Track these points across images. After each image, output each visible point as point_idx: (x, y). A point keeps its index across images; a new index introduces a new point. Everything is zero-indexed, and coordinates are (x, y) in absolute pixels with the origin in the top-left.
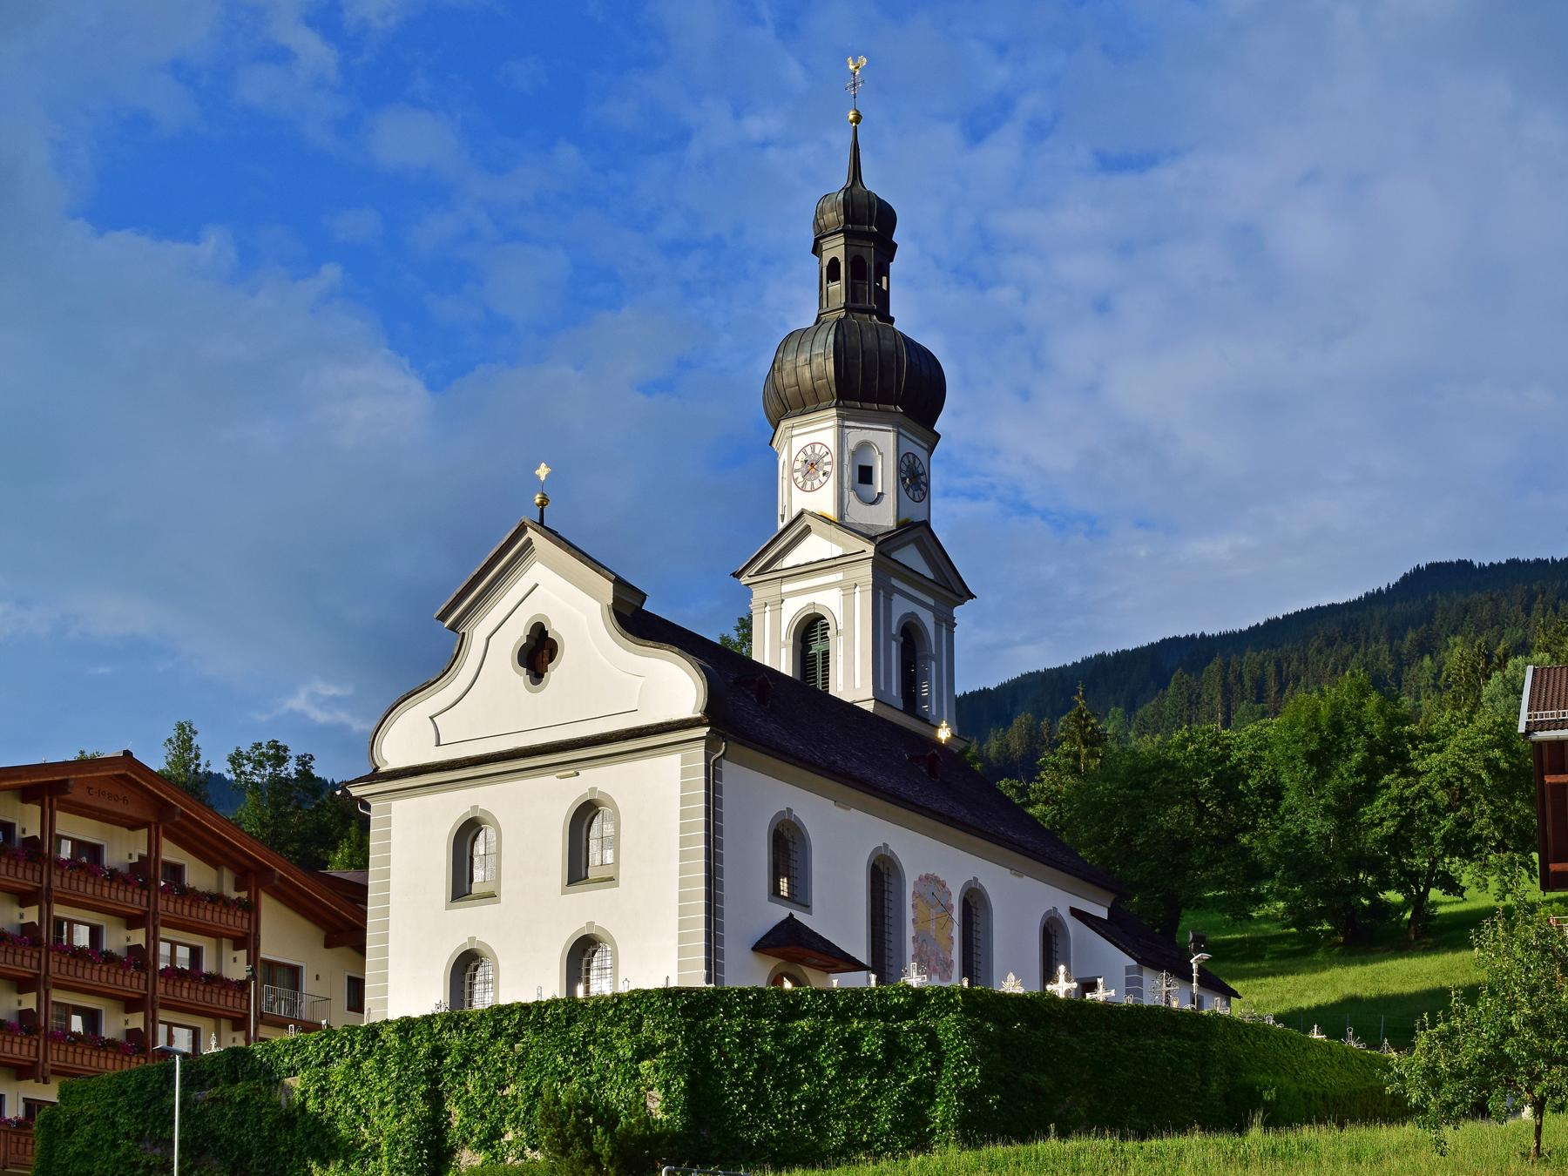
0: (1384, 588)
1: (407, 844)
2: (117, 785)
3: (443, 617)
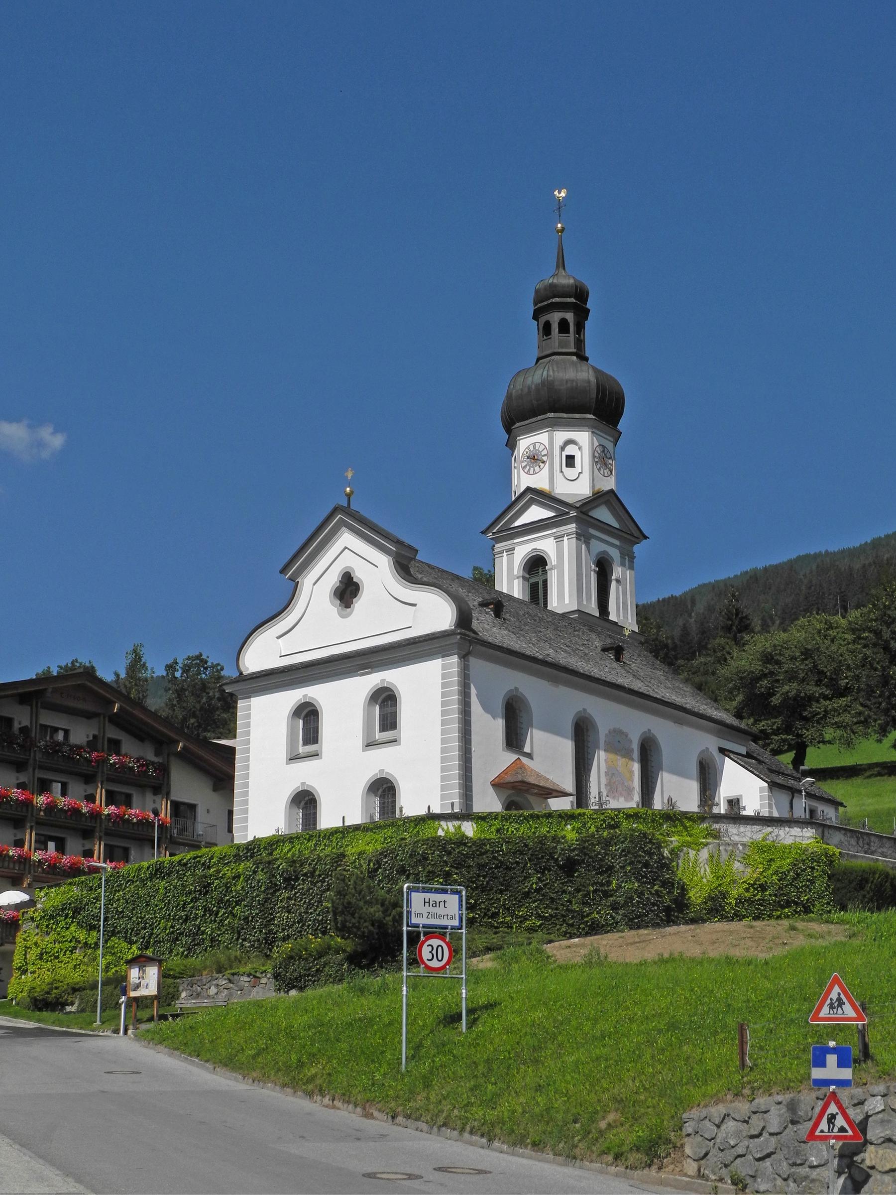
1: (264, 721)
2: (77, 688)
3: (283, 571)
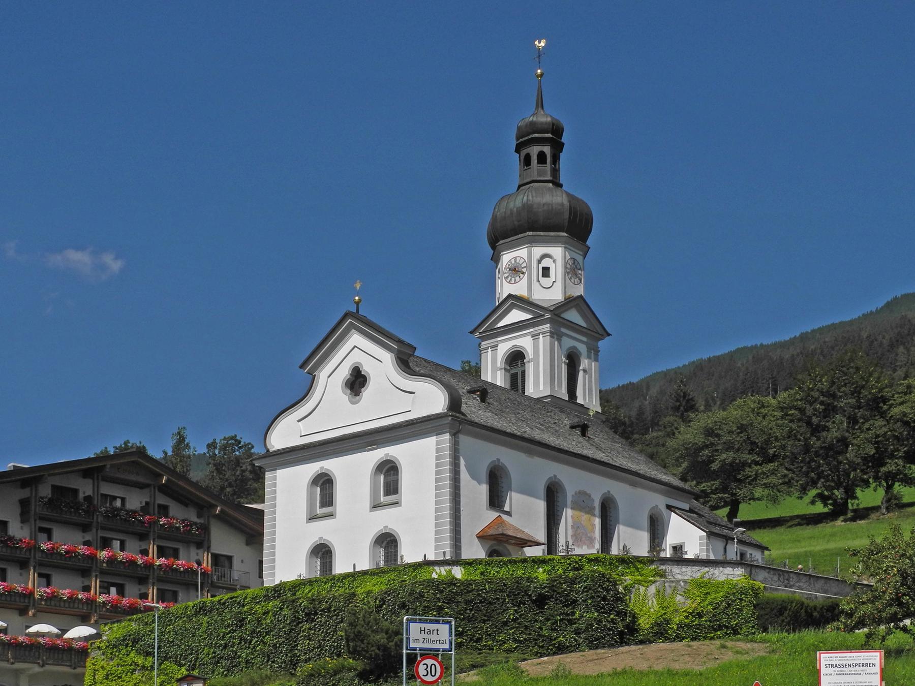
0: (874, 310)
1: (287, 489)
3: (303, 366)
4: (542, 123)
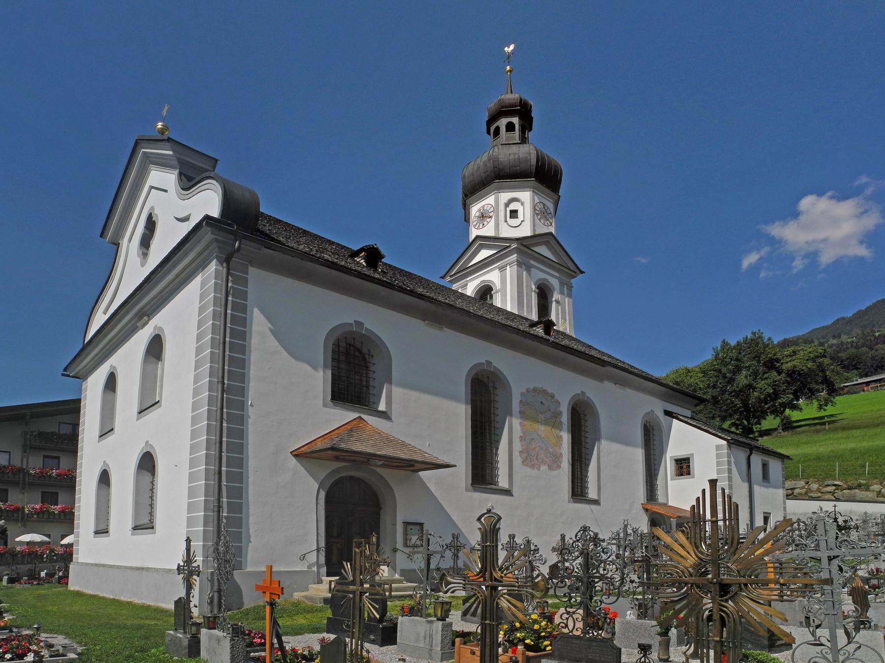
4: (510, 99)
